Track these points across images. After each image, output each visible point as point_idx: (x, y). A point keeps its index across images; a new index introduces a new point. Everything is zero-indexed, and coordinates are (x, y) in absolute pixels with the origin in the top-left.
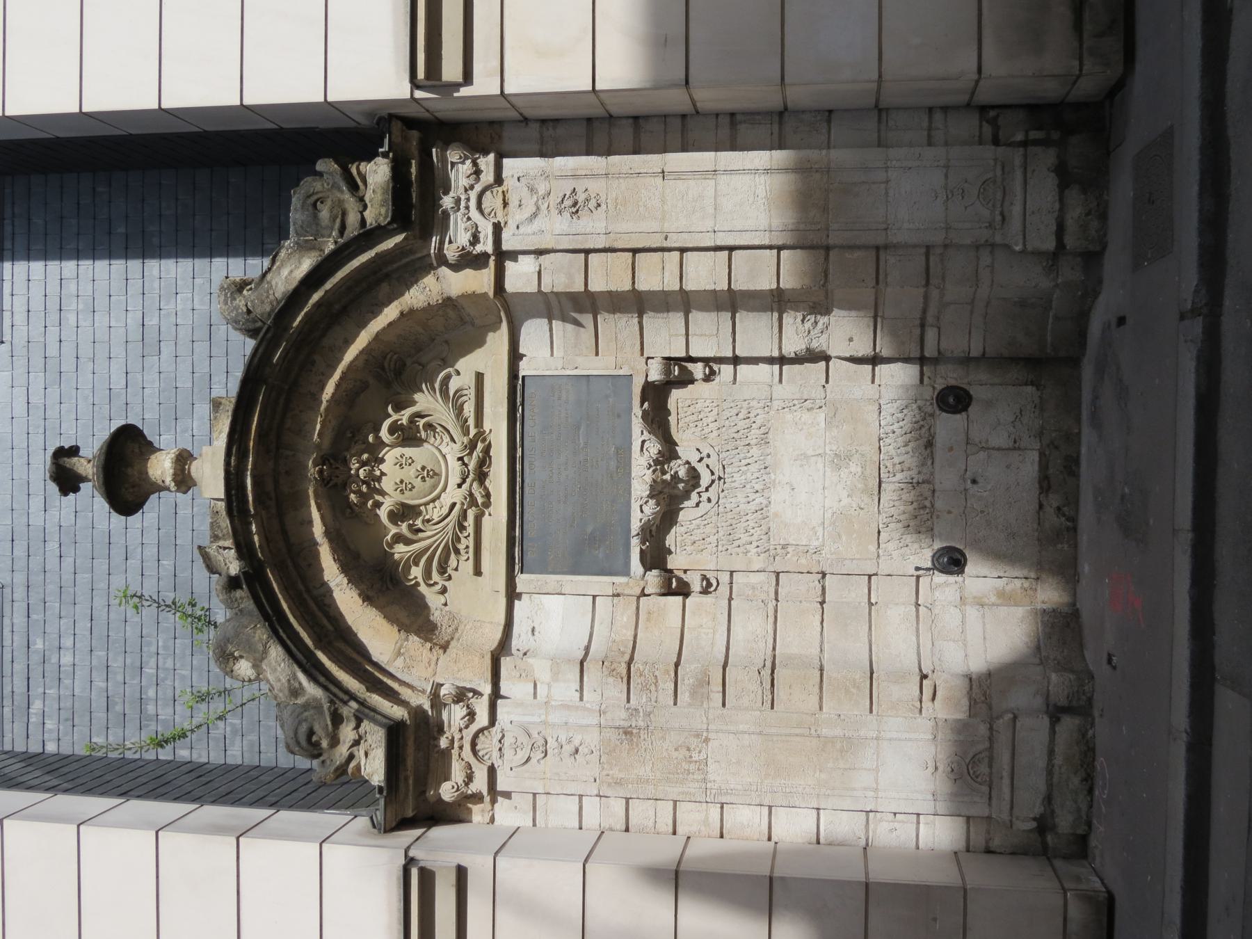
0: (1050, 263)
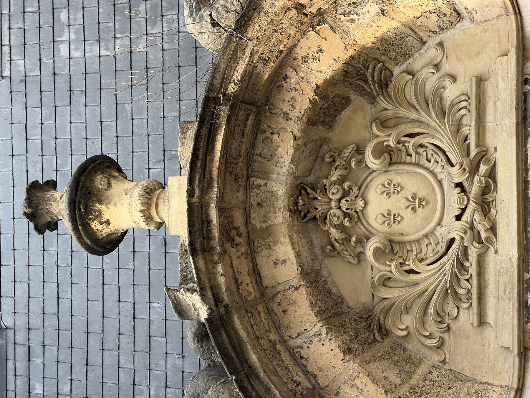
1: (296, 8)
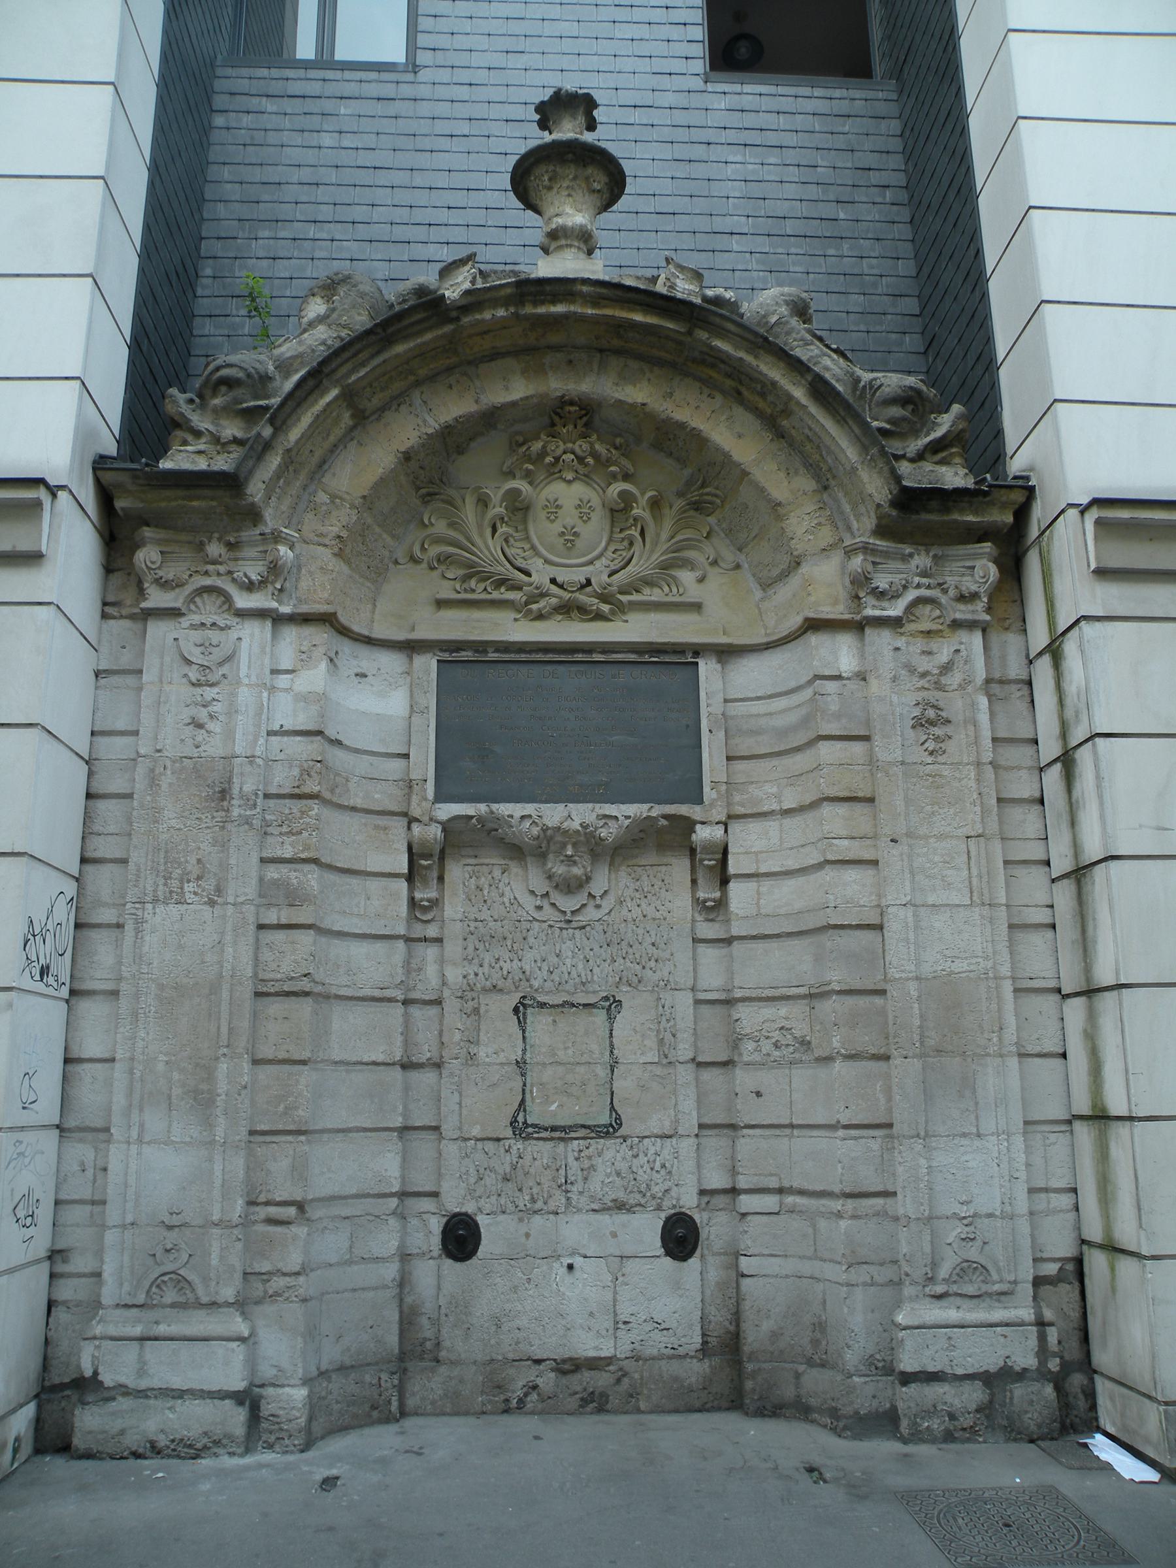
0: (880, 1365)
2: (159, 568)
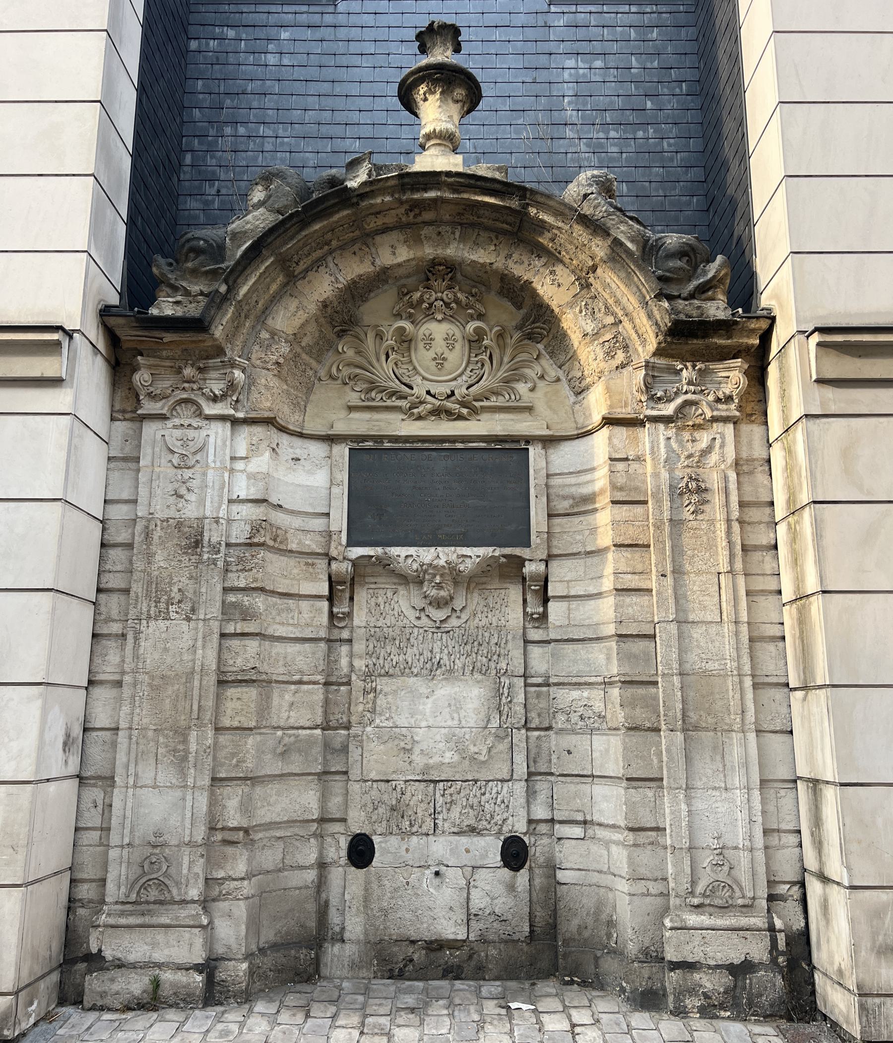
1: (593, 265)
2: (150, 385)
